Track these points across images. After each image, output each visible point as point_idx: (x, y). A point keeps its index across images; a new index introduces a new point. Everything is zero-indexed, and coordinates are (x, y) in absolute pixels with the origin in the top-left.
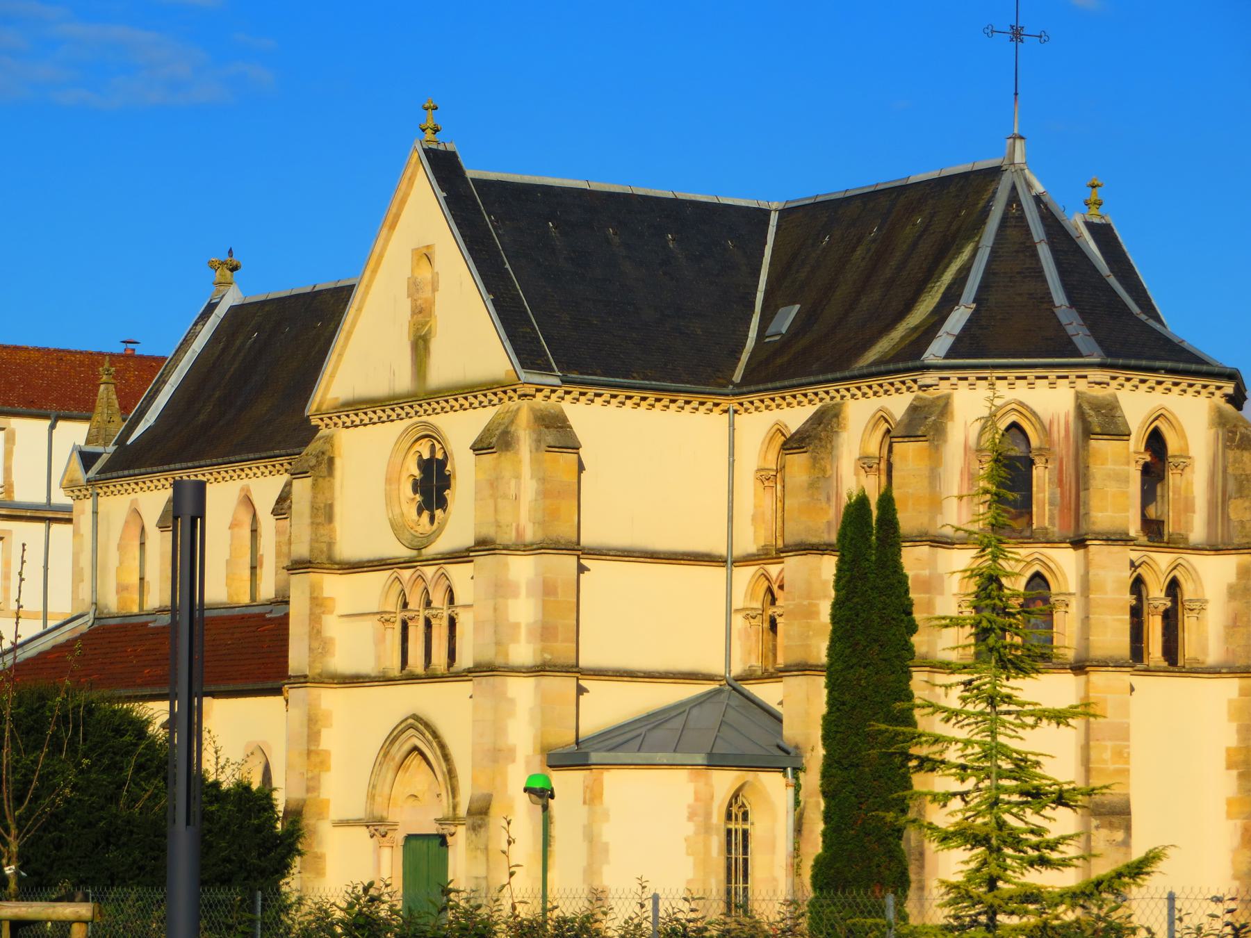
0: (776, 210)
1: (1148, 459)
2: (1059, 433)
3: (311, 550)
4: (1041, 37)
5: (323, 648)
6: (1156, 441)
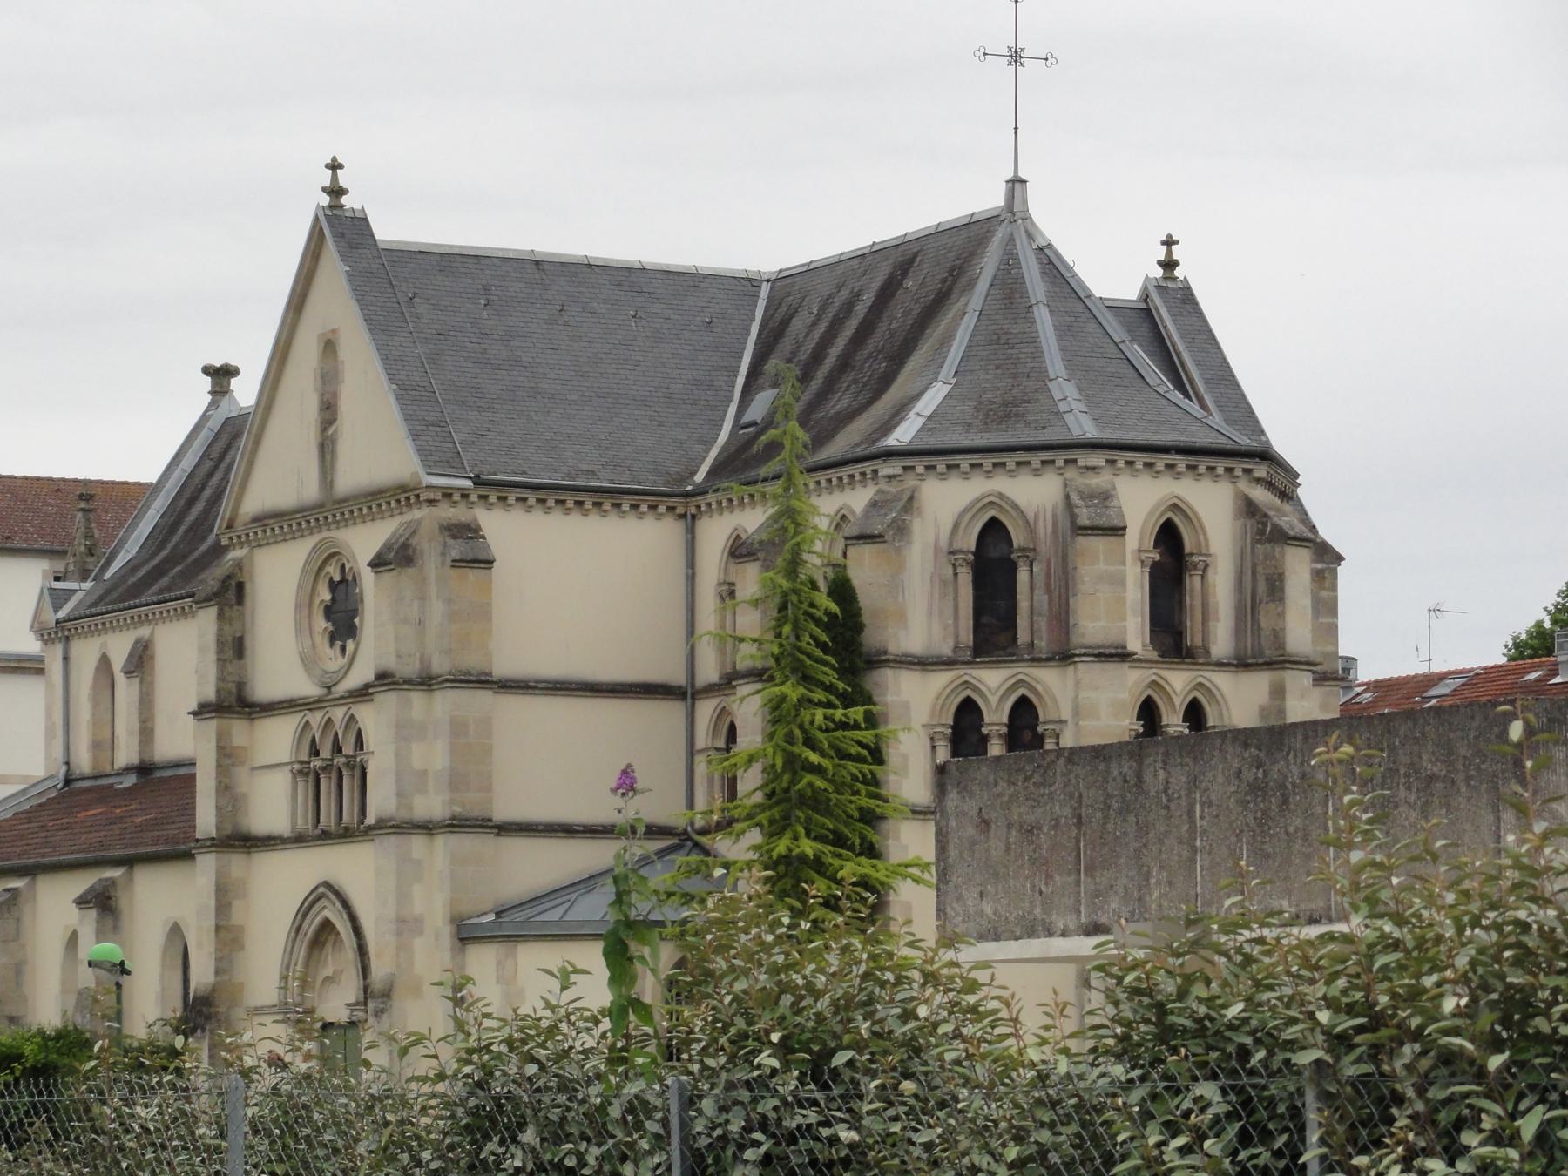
0: (768, 281)
1: (1158, 557)
2: (1044, 530)
3: (218, 691)
4: (985, 54)
5: (234, 806)
6: (1168, 536)
